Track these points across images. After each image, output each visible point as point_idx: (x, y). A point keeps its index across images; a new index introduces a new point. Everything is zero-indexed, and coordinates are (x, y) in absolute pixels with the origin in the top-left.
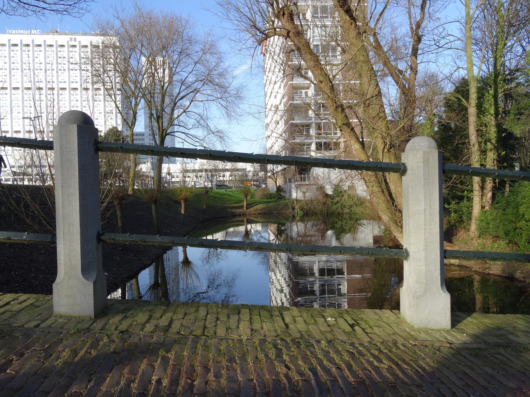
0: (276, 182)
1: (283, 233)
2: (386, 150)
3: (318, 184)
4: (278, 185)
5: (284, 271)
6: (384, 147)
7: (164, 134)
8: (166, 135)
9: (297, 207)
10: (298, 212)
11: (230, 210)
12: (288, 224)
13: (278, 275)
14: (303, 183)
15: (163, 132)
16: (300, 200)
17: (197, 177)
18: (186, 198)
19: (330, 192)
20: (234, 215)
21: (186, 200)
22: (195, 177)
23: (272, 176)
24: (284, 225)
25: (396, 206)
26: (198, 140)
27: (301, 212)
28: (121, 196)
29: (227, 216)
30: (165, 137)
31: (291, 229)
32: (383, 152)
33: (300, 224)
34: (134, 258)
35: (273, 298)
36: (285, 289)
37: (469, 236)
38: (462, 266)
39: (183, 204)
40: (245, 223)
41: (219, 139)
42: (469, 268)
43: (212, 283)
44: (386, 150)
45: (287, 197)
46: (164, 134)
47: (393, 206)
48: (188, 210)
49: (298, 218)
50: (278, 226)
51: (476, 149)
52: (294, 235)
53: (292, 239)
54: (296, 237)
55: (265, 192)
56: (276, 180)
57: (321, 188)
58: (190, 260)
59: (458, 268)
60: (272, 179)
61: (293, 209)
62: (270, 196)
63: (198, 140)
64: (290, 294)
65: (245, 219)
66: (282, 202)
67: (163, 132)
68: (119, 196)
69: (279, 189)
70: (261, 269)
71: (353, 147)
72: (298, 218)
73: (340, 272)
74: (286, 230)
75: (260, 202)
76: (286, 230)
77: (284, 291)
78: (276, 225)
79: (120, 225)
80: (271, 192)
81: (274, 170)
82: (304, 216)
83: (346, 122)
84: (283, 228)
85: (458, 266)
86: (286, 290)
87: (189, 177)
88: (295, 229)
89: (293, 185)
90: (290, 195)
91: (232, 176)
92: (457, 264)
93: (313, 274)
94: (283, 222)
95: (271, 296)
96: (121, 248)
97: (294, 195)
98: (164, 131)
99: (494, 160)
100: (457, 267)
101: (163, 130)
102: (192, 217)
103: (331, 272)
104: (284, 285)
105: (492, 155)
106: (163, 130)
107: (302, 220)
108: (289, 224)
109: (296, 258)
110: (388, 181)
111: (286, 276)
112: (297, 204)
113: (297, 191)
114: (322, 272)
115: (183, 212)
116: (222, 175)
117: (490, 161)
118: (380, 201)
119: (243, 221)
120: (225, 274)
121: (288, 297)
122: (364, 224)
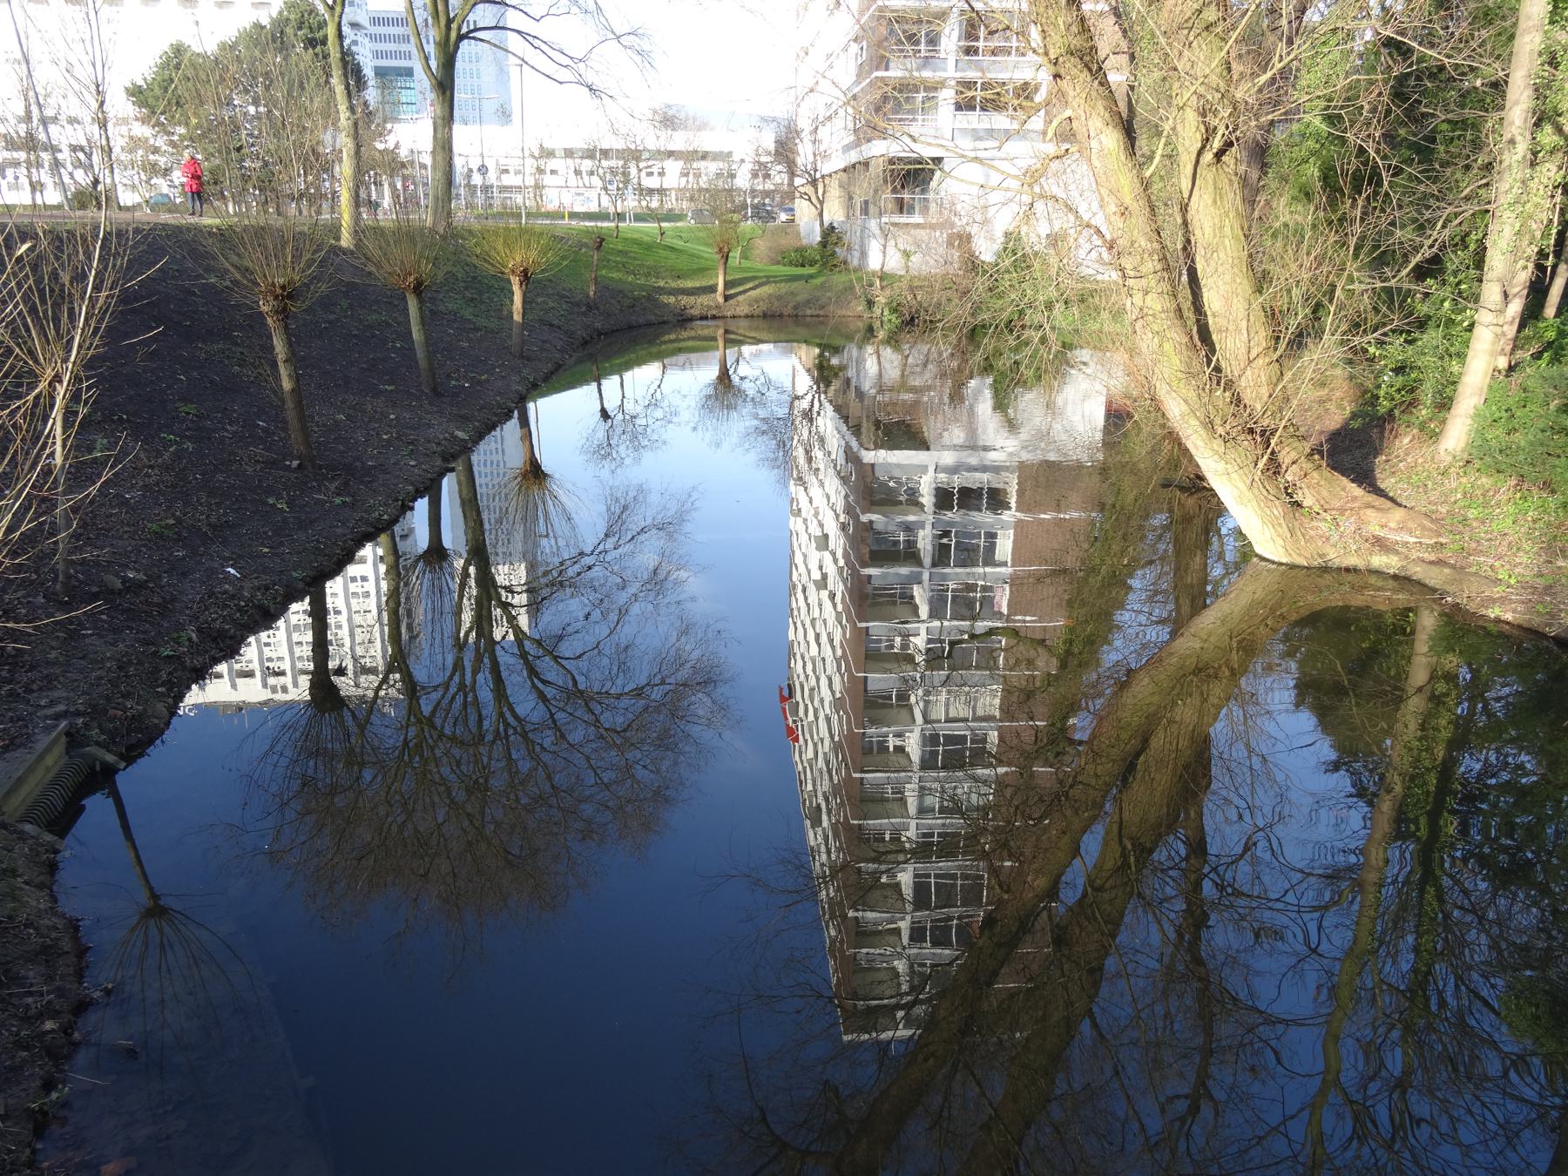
0: (821, 215)
1: (836, 375)
2: (1208, 157)
3: (953, 225)
4: (826, 224)
5: (833, 485)
6: (1203, 147)
7: (453, 35)
8: (461, 38)
9: (882, 300)
10: (883, 315)
11: (672, 300)
12: (852, 351)
13: (815, 491)
14: (904, 219)
15: (448, 28)
16: (892, 276)
17: (577, 172)
18: (525, 272)
19: (986, 250)
20: (684, 320)
21: (526, 276)
22: (572, 175)
23: (809, 189)
24: (837, 350)
25: (1218, 369)
26: (566, 61)
27: (893, 317)
28: (283, 287)
29: (665, 322)
30: (457, 48)
31: (860, 362)
32: (1197, 162)
33: (887, 352)
34: (338, 501)
35: (799, 559)
36: (830, 581)
37: (1433, 458)
38: (1407, 579)
39: (516, 289)
40: (721, 344)
41: (638, 59)
42: (1434, 590)
43: (617, 522)
44: (1208, 157)
45: (855, 262)
46: (453, 35)
47: (1209, 366)
48: (540, 300)
49: (881, 335)
50: (821, 355)
51: (1519, 157)
52: (868, 386)
53: (860, 394)
54: (873, 391)
55: (786, 242)
56: (821, 203)
57: (962, 240)
58: (546, 466)
59: (1391, 584)
60: (810, 200)
61: (870, 304)
62: (801, 257)
63: (566, 61)
64: (846, 555)
65: (721, 331)
66: (839, 279)
67: (448, 28)
68: (273, 285)
69: (829, 232)
70: (766, 478)
71: (1094, 144)
72: (881, 335)
73: (996, 500)
74: (843, 368)
75: (768, 277)
76: (843, 368)
77: (830, 586)
78: (817, 351)
79: (287, 385)
80: (805, 242)
81: (816, 171)
82: (900, 328)
83: (1077, 42)
84: (835, 361)
85: (1395, 577)
86: (838, 542)
87: (553, 172)
88: (871, 366)
89: (873, 224)
90: (864, 254)
91: (687, 175)
92: (1391, 571)
93: (913, 500)
94: (837, 342)
95: (793, 552)
96: (295, 463)
97: (874, 263)
98: (454, 26)
99: (1555, 187)
100: (1391, 582)
101: (449, 22)
102: (551, 325)
103: (969, 498)
104: (832, 528)
105: (1554, 169)
106: (449, 22)
107: (893, 340)
108: (855, 352)
109: (869, 456)
110: (1199, 267)
111: (840, 506)
112: (882, 288)
113: (885, 247)
114: (944, 498)
115: (517, 317)
116: (655, 170)
117: (1541, 192)
118: (1168, 347)
119: (714, 339)
120: (654, 498)
121: (841, 563)
122: (1085, 364)
